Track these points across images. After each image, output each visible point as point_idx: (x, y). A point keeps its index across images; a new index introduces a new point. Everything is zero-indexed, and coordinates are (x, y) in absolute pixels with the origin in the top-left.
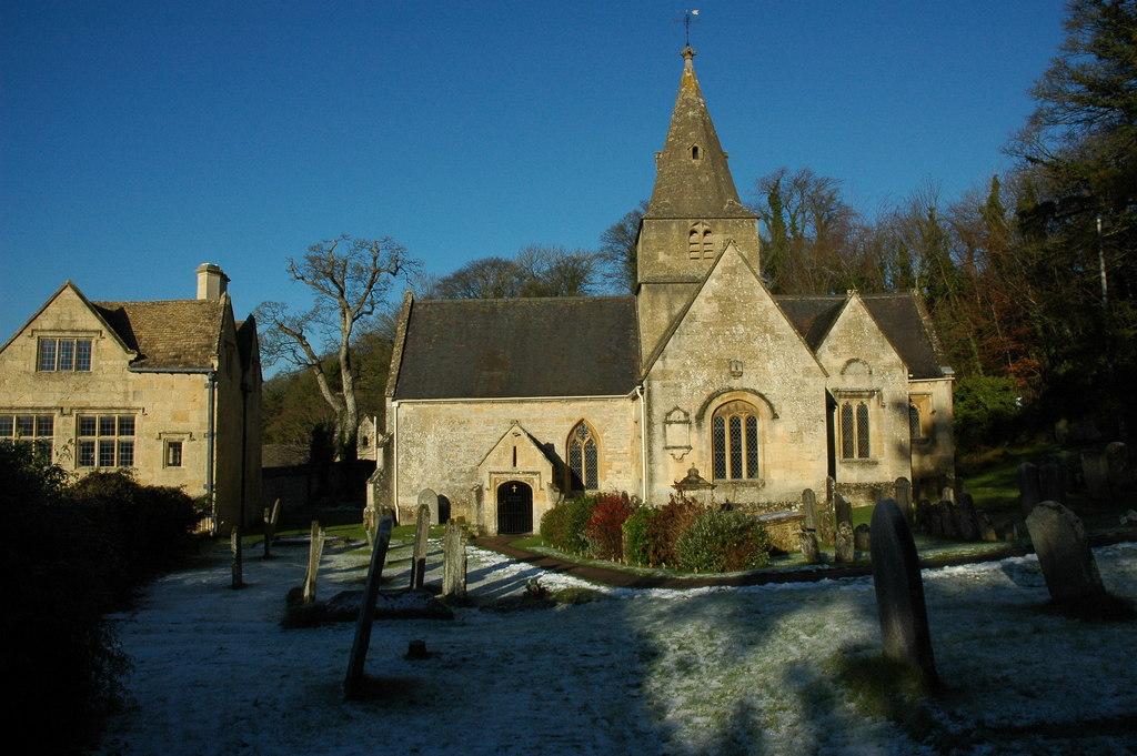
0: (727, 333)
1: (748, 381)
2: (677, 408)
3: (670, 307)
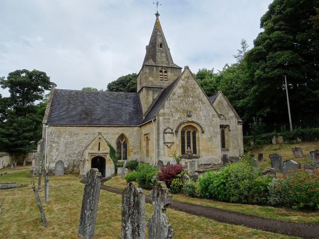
1: (194, 118)
3: (153, 97)
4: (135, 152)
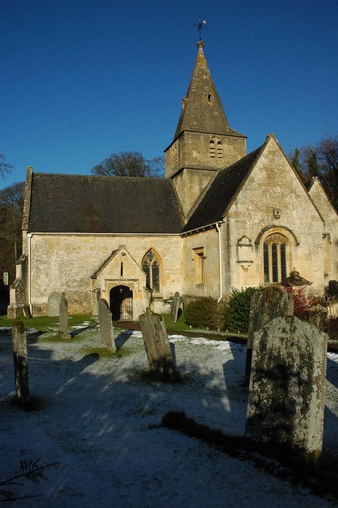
0: (271, 191)
1: (282, 222)
2: (244, 236)
3: (201, 184)
4: (173, 279)
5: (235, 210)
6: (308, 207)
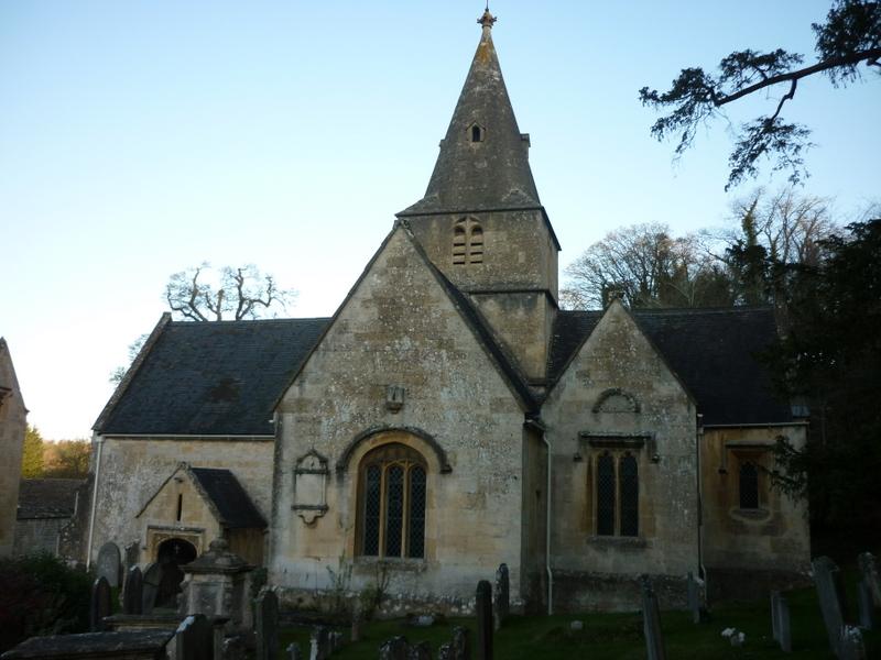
0: (388, 348)
1: (411, 418)
5: (297, 396)
6: (483, 379)
